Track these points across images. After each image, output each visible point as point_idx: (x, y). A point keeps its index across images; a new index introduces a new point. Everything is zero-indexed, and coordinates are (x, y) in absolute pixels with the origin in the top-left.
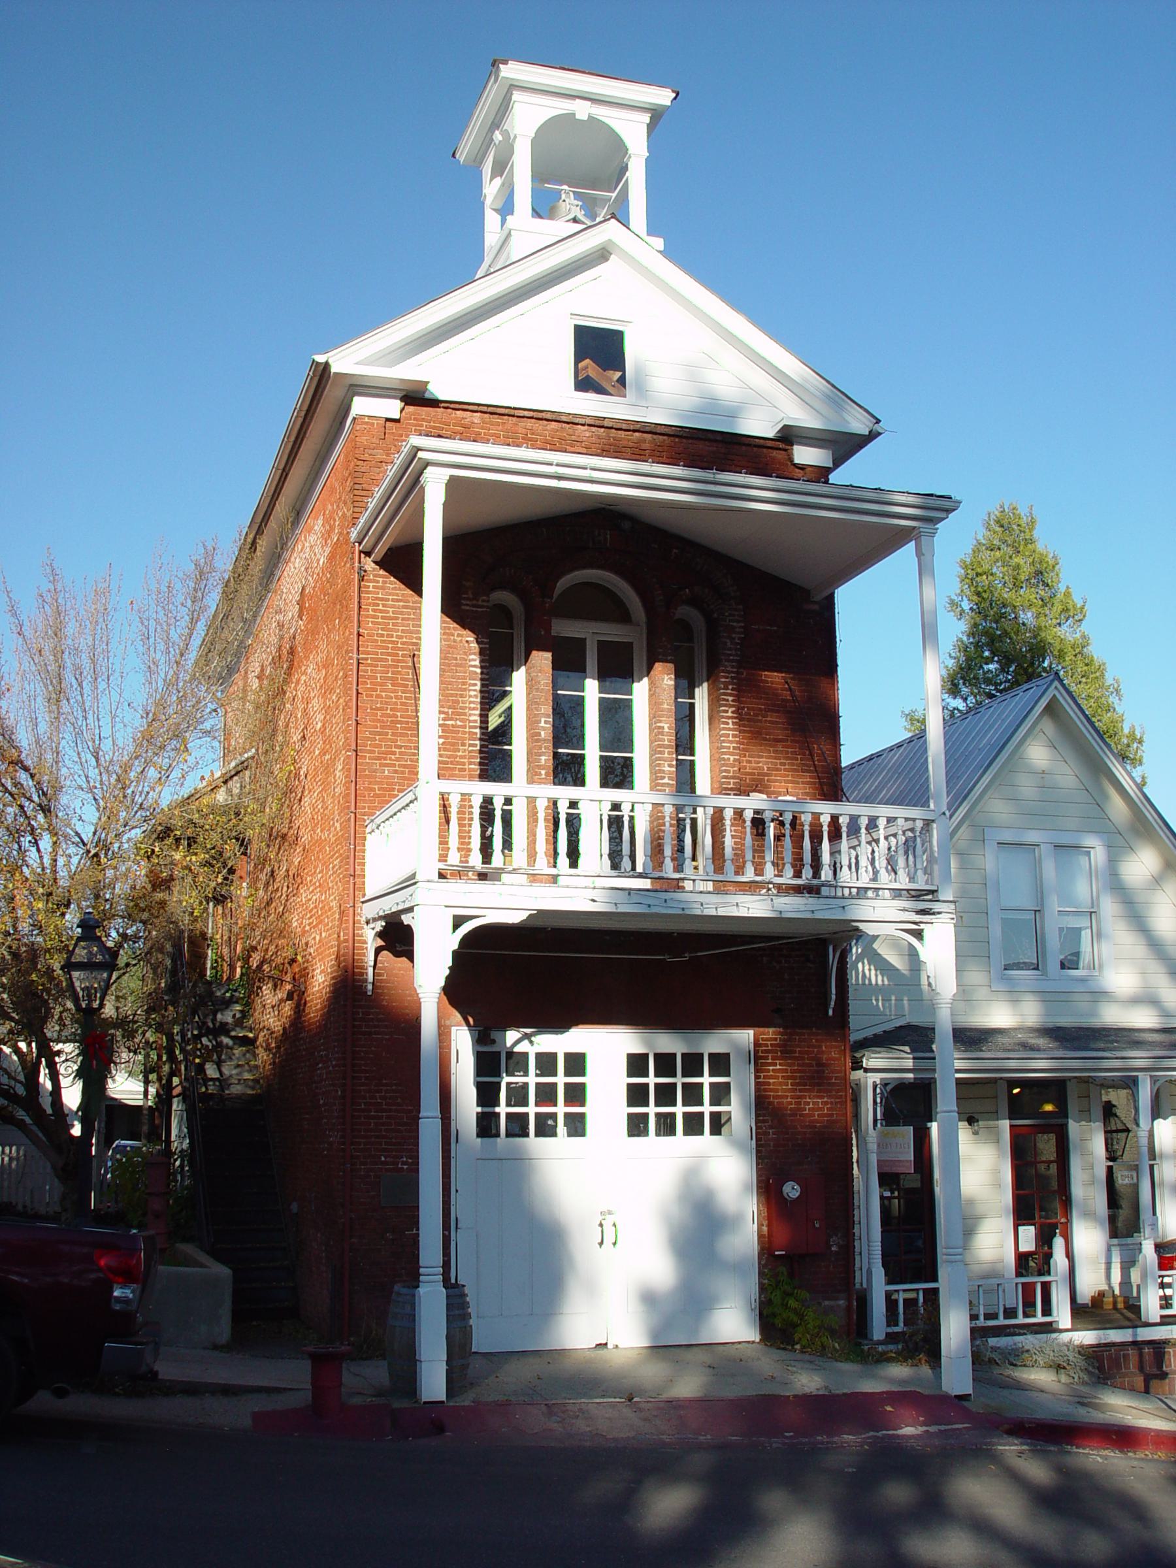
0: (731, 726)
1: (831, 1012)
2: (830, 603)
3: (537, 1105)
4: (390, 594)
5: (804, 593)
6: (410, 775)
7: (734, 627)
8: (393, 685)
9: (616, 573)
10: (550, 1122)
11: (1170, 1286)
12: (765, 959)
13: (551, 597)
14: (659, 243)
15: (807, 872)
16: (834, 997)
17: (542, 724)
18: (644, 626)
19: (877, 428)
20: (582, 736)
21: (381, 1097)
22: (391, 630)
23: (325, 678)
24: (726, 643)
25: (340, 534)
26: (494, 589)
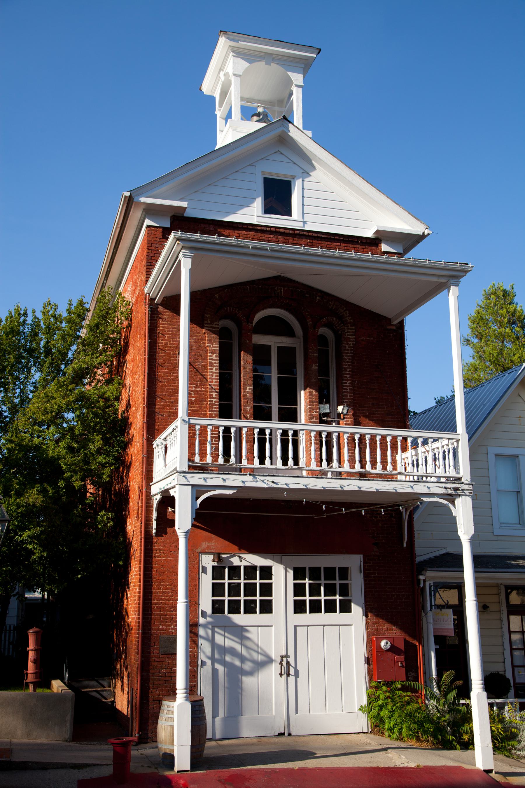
0: (348, 391)
1: (405, 545)
2: (401, 324)
5: (388, 320)
6: (175, 415)
7: (349, 338)
8: (168, 369)
9: (287, 310)
13: (252, 323)
14: (309, 133)
16: (406, 537)
17: (248, 390)
18: (302, 338)
21: (160, 592)
22: (167, 340)
23: (133, 367)
25: (140, 290)
26: (221, 319)
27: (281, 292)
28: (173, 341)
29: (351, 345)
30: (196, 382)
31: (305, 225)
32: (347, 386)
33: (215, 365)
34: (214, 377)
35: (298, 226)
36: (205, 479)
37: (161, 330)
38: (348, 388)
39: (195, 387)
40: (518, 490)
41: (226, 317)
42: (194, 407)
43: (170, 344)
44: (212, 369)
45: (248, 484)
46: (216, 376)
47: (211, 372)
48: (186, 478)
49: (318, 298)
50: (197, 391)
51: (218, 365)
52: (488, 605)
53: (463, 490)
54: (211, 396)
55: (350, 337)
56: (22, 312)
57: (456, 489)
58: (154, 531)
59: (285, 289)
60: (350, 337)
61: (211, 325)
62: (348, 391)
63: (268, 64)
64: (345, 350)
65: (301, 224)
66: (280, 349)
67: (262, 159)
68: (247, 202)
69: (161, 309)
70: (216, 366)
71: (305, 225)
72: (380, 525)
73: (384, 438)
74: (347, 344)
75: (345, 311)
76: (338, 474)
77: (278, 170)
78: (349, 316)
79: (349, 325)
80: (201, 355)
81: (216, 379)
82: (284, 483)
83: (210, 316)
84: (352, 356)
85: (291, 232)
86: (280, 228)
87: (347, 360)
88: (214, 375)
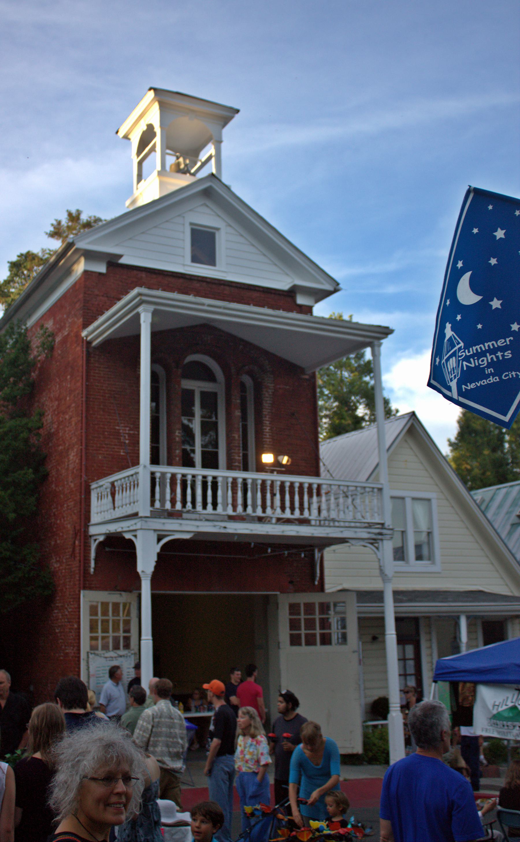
3: (305, 629)
5: (302, 370)
15: (297, 512)
19: (337, 288)
39: (129, 430)
40: (403, 529)
50: (130, 434)
52: (377, 636)
73: (283, 484)
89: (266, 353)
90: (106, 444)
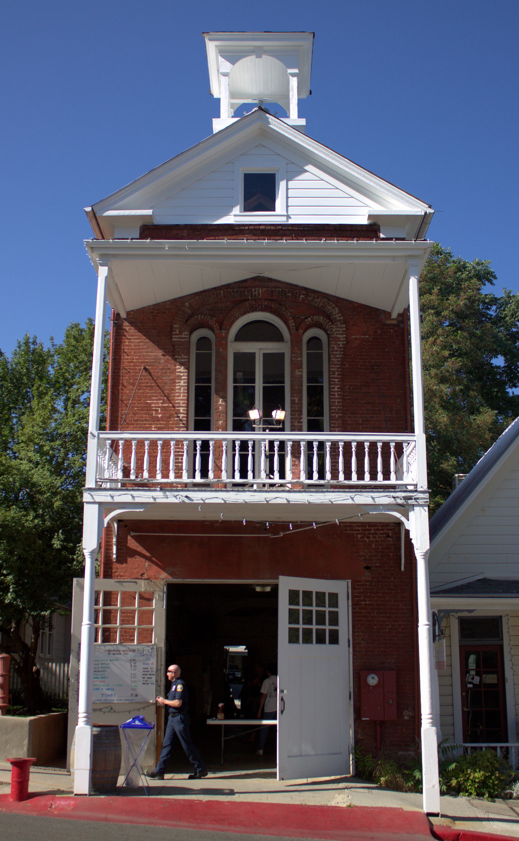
0: (337, 396)
1: (403, 569)
4: (132, 336)
7: (339, 338)
10: (131, 622)
11: (217, 716)
12: (359, 536)
17: (220, 403)
18: (289, 342)
20: (308, 423)
24: (334, 348)
27: (259, 293)
28: (139, 356)
29: (341, 346)
30: (163, 398)
31: (289, 220)
32: (335, 392)
33: (183, 378)
34: (182, 391)
35: (282, 220)
36: (112, 497)
37: (127, 345)
38: (336, 394)
39: (162, 403)
41: (202, 325)
42: (160, 424)
43: (136, 359)
44: (180, 382)
45: (158, 501)
46: (184, 390)
47: (179, 386)
48: (91, 495)
49: (302, 296)
50: (164, 407)
51: (186, 378)
53: (415, 499)
54: (178, 412)
55: (340, 336)
56: (31, 340)
57: (406, 498)
58: (115, 556)
59: (264, 290)
60: (340, 336)
61: (180, 336)
62: (337, 396)
63: (259, 56)
64: (333, 351)
65: (284, 219)
66: (266, 356)
67: (242, 155)
68: (227, 212)
69: (126, 324)
70: (184, 379)
71: (289, 220)
72: (373, 546)
74: (336, 344)
75: (333, 308)
76: (261, 485)
77: (259, 167)
78: (338, 314)
79: (339, 323)
80: (169, 369)
81: (183, 393)
82: (221, 497)
83: (178, 326)
84: (341, 358)
85: (272, 228)
86: (260, 225)
87: (336, 363)
88: (182, 388)
89: (337, 301)
90: (134, 420)
